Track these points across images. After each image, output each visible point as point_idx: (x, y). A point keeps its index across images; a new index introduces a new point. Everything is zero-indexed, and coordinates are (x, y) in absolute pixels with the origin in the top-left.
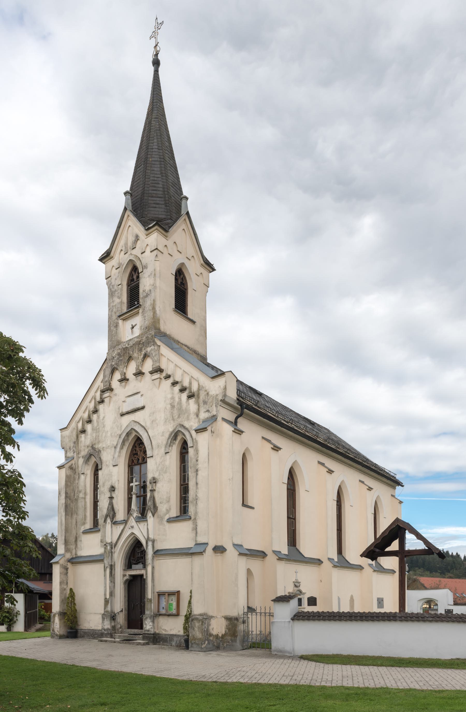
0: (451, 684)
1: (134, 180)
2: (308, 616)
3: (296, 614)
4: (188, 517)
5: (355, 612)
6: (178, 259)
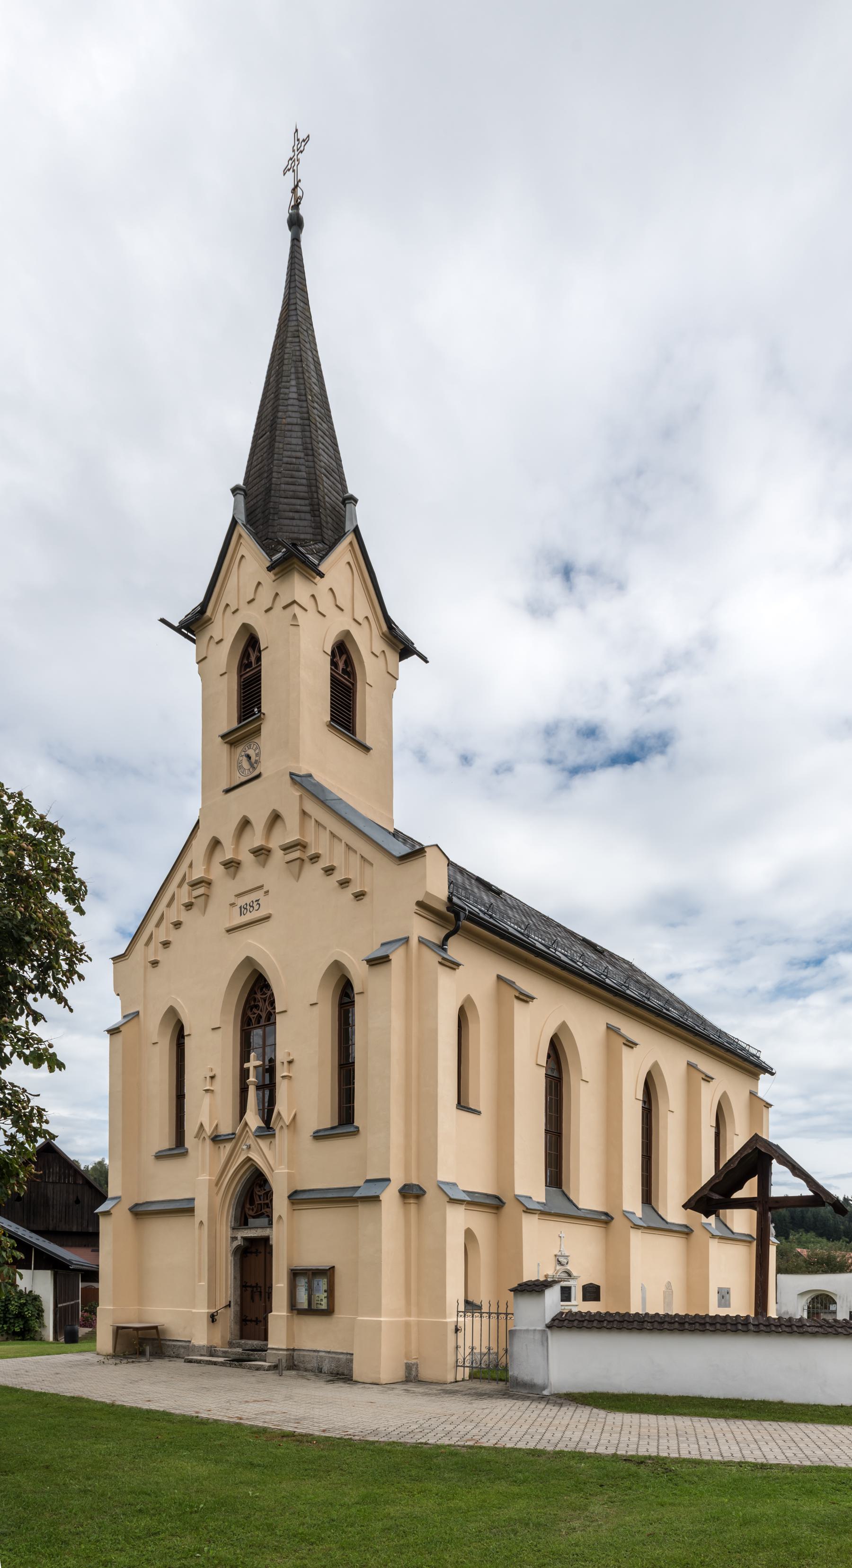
0: (830, 1457)
1: (252, 463)
2: (580, 1321)
3: (555, 1316)
4: (352, 1129)
5: (711, 1314)
6: (337, 624)
